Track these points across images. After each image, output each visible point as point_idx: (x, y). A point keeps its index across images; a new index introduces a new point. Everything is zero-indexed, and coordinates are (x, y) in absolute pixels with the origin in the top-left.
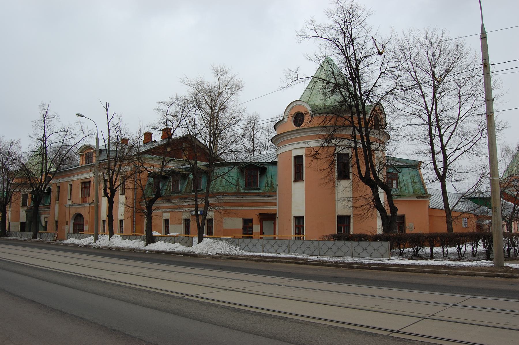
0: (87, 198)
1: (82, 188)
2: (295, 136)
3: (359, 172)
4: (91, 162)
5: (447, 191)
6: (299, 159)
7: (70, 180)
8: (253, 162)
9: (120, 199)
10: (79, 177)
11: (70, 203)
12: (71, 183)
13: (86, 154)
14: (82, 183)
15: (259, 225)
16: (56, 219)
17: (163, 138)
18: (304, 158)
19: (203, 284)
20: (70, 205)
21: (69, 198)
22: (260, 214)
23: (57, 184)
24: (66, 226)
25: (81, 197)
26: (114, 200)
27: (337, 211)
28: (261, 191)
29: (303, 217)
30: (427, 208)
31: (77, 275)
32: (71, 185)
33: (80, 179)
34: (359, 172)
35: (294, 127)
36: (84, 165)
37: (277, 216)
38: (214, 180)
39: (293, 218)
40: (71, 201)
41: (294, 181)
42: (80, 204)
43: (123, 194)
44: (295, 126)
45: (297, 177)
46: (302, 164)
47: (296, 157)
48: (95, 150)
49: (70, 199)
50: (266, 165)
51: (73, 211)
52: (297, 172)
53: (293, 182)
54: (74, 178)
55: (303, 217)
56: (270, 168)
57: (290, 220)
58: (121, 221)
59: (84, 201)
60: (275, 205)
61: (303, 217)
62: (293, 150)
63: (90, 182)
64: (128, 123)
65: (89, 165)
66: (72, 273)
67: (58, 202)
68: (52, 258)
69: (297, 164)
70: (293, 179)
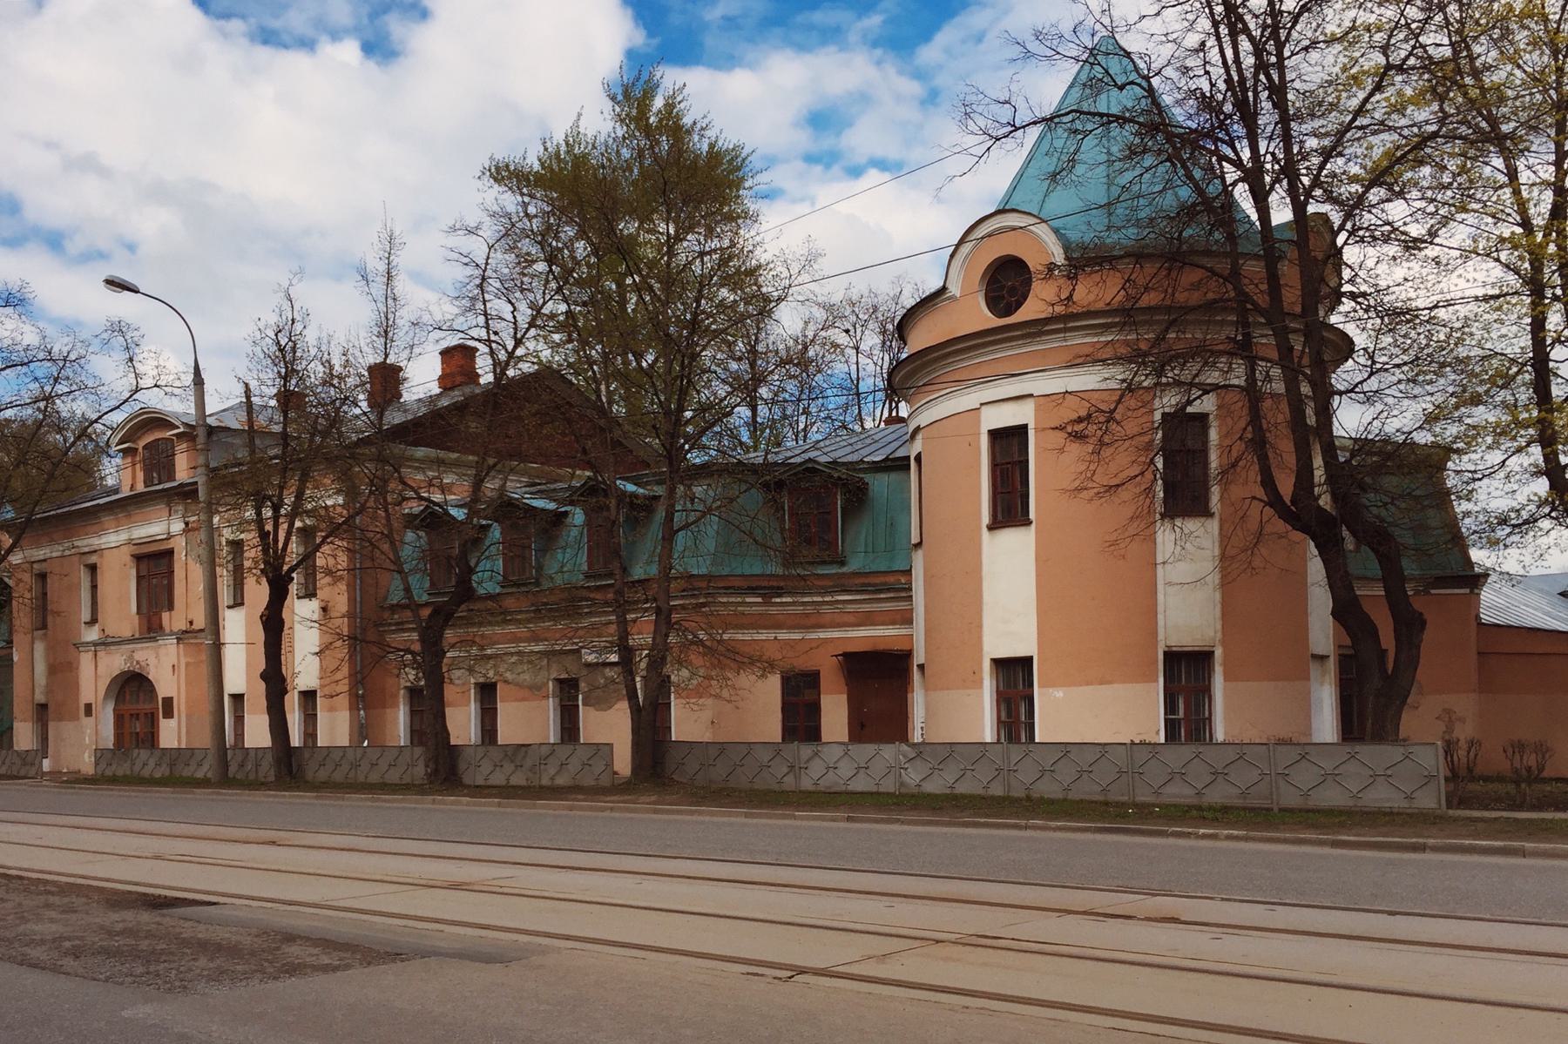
0: (165, 616)
1: (139, 579)
2: (992, 352)
3: (1268, 482)
4: (172, 478)
5: (266, 718)
6: (1009, 442)
7: (86, 550)
8: (819, 463)
9: (302, 612)
10: (123, 536)
11: (92, 635)
12: (93, 559)
13: (145, 447)
14: (138, 558)
15: (845, 696)
16: (40, 697)
17: (446, 382)
18: (1031, 434)
19: (1319, 978)
20: (95, 644)
21: (86, 615)
22: (845, 655)
23: (35, 566)
24: (1166, 537)
25: (138, 613)
26: (285, 615)
27: (1161, 636)
28: (845, 569)
29: (1028, 661)
30: (1474, 624)
31: (56, 878)
32: (93, 569)
33: (130, 542)
34: (1268, 482)
35: (990, 320)
36: (140, 488)
37: (919, 657)
38: (686, 526)
39: (987, 666)
40: (96, 627)
41: (991, 528)
42: (137, 636)
43: (310, 594)
44: (990, 314)
45: (999, 509)
46: (1021, 462)
47: (995, 435)
48: (182, 430)
49: (93, 621)
50: (864, 471)
51: (115, 663)
52: (999, 490)
53: (985, 530)
54: (104, 539)
55: (1031, 658)
56: (879, 485)
57: (977, 673)
58: (309, 696)
59: (151, 629)
60: (907, 620)
61: (1031, 658)
62: (983, 407)
63: (170, 552)
64: (685, 85)
65: (163, 490)
66: (164, 887)
67: (45, 635)
68: (53, 836)
69: (999, 460)
70: (986, 519)
